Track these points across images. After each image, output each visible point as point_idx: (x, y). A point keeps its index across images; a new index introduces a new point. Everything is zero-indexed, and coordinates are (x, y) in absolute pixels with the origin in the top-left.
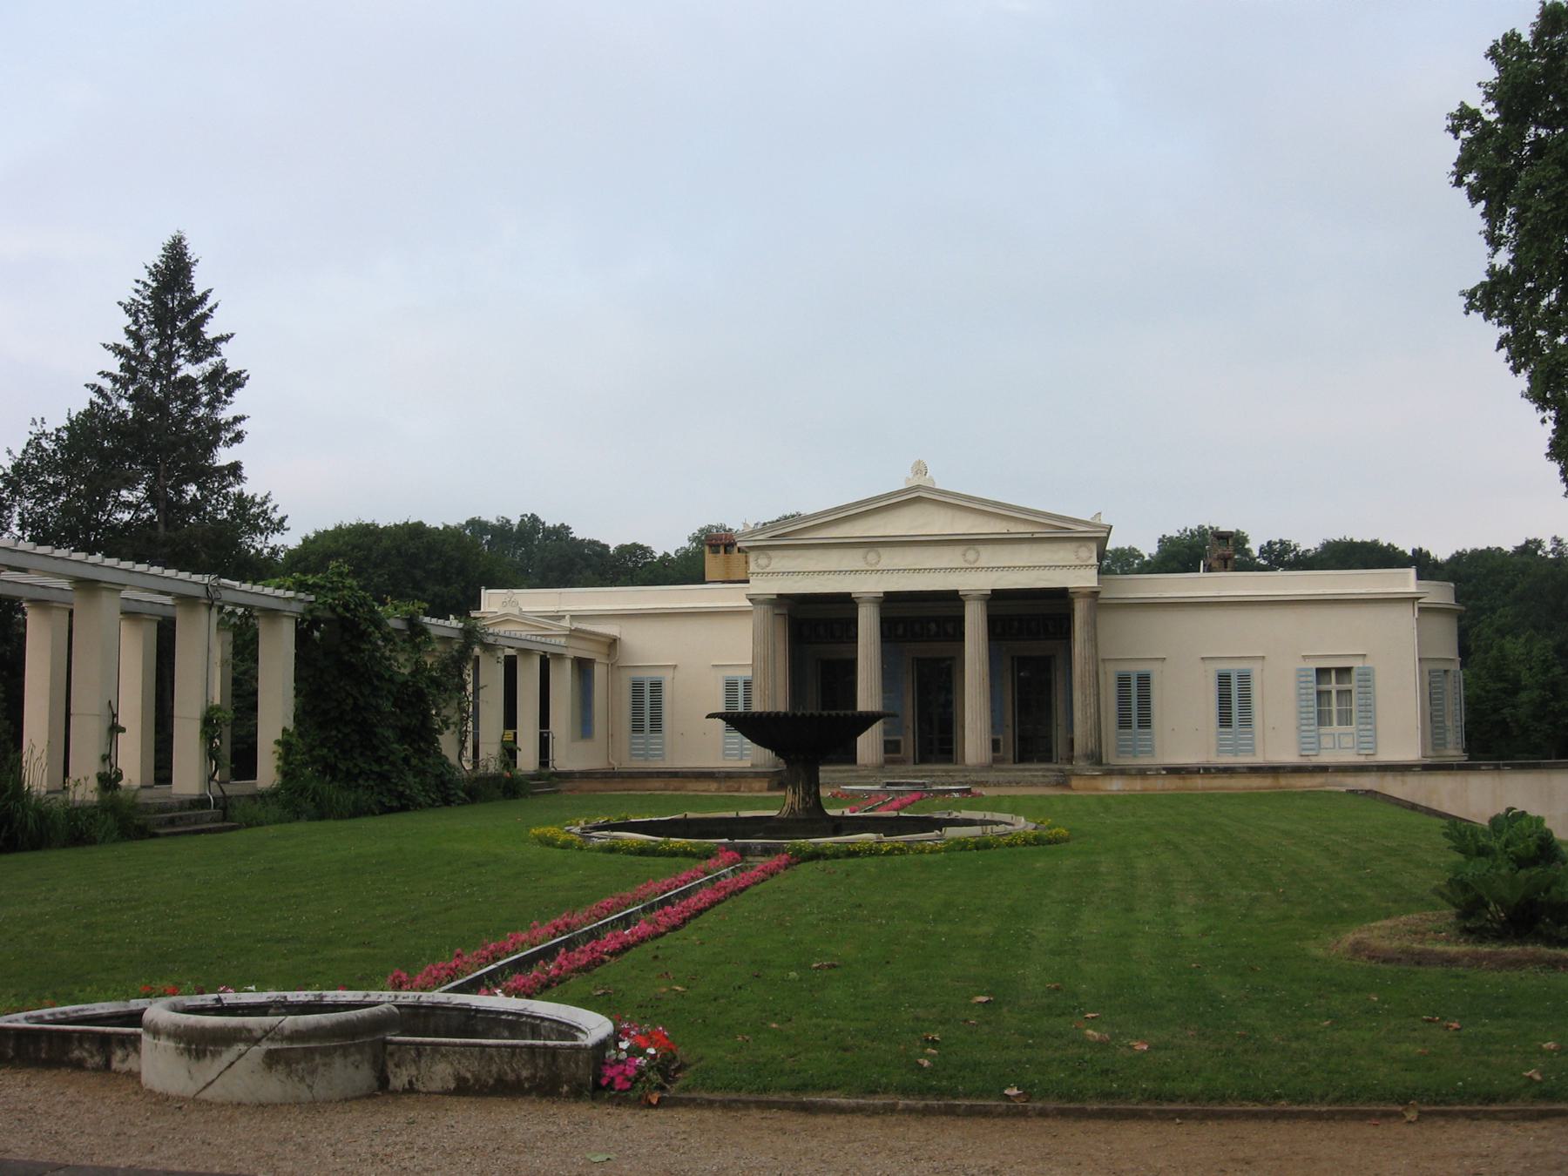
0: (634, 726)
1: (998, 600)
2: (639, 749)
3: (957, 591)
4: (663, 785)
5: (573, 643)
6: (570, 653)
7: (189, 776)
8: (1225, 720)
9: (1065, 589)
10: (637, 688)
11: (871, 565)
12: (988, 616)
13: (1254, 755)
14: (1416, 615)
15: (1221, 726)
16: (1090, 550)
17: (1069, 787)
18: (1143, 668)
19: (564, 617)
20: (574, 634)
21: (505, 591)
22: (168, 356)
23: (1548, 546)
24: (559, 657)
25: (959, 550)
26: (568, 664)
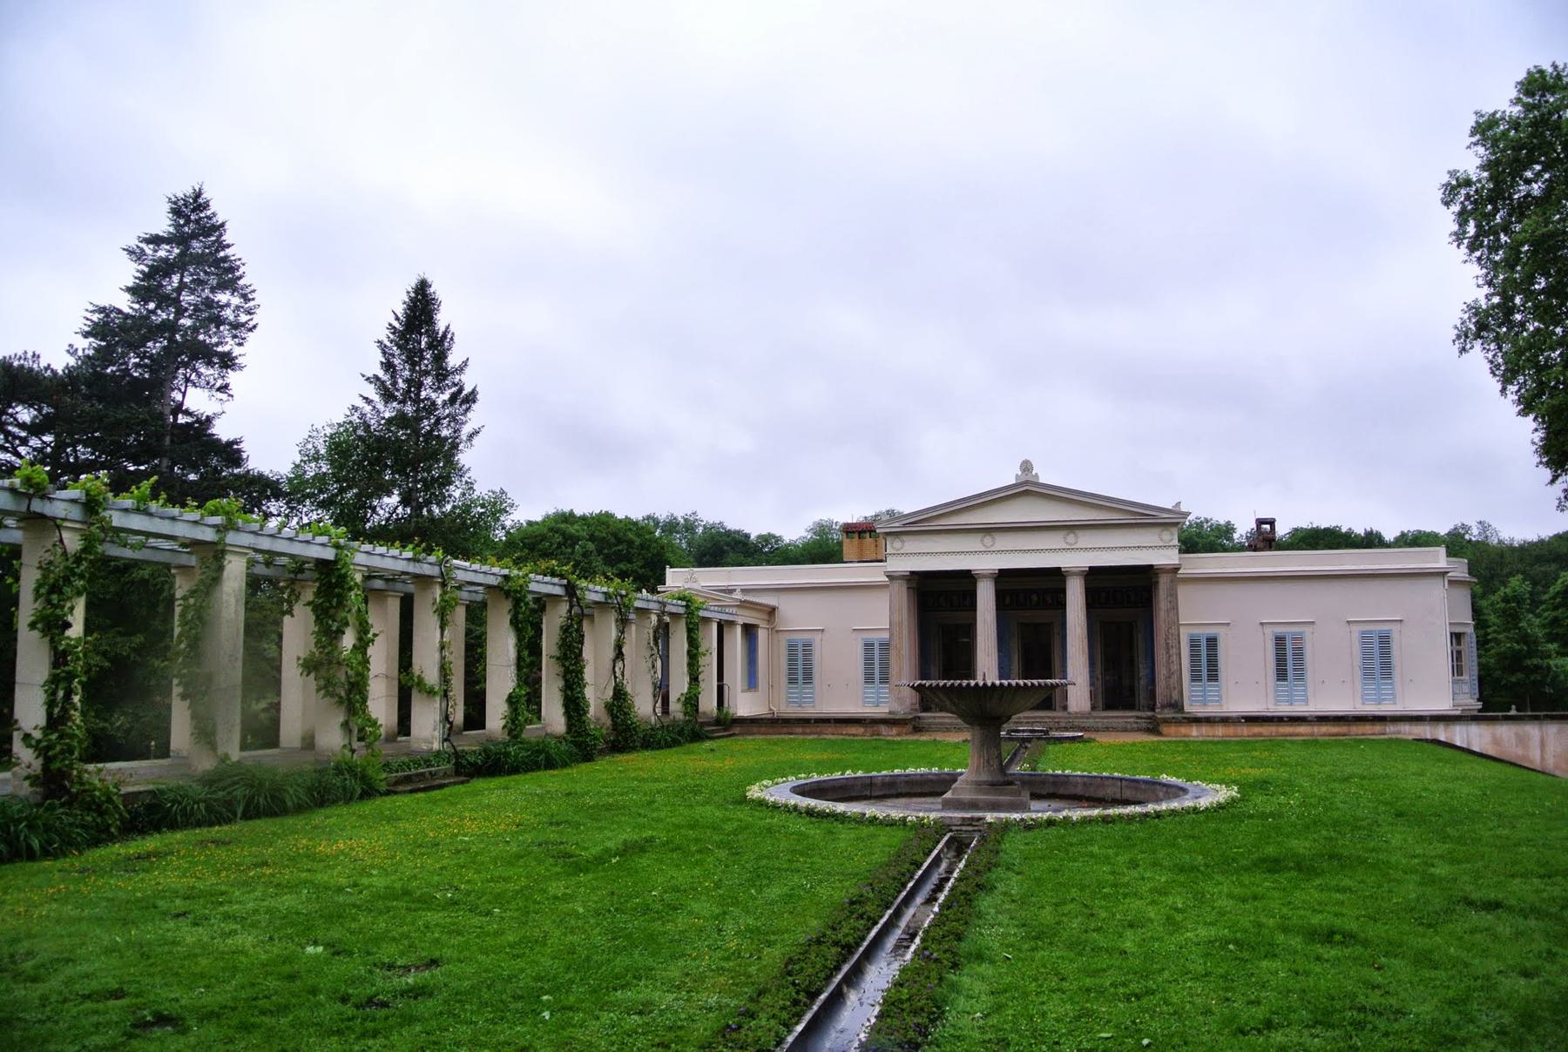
1: (1095, 576)
3: (1060, 568)
5: (740, 612)
6: (741, 621)
7: (427, 726)
8: (1281, 674)
10: (792, 648)
11: (1071, 544)
12: (996, 591)
13: (1307, 704)
15: (1278, 680)
16: (1172, 534)
17: (1159, 734)
18: (1211, 631)
19: (735, 590)
20: (744, 605)
22: (415, 384)
23: (1475, 531)
24: (732, 623)
25: (1062, 534)
26: (739, 629)
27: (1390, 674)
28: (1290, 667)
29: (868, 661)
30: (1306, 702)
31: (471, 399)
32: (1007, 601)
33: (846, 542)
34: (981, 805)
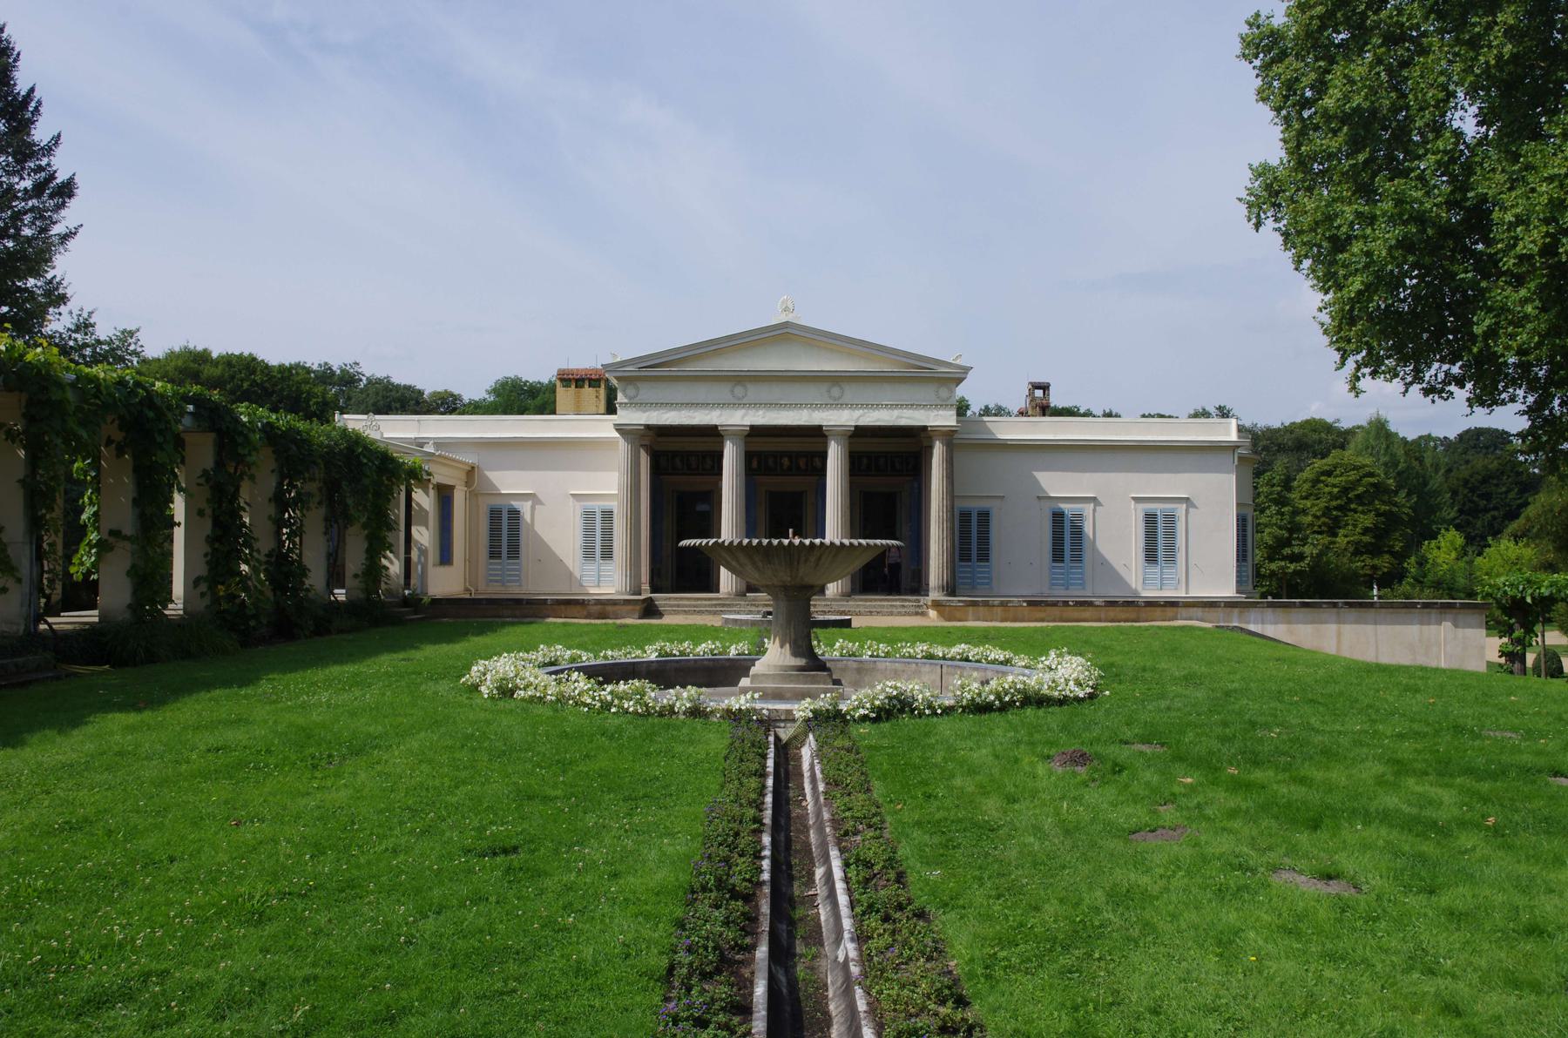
0: (491, 552)
1: (860, 432)
2: (495, 575)
4: (1133, 616)
8: (1058, 555)
9: (820, 427)
10: (495, 515)
11: (739, 399)
14: (1236, 463)
15: (1054, 561)
21: (365, 417)
25: (824, 387)
27: (988, 555)
28: (1067, 547)
29: (588, 532)
30: (1083, 585)
31: (66, 190)
32: (755, 464)
33: (560, 390)
34: (788, 695)
